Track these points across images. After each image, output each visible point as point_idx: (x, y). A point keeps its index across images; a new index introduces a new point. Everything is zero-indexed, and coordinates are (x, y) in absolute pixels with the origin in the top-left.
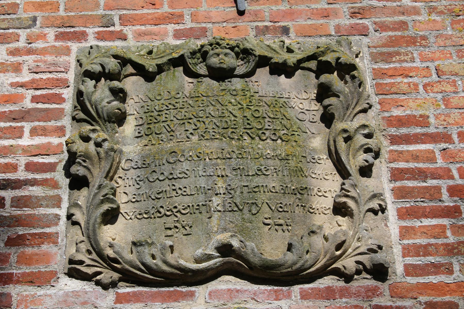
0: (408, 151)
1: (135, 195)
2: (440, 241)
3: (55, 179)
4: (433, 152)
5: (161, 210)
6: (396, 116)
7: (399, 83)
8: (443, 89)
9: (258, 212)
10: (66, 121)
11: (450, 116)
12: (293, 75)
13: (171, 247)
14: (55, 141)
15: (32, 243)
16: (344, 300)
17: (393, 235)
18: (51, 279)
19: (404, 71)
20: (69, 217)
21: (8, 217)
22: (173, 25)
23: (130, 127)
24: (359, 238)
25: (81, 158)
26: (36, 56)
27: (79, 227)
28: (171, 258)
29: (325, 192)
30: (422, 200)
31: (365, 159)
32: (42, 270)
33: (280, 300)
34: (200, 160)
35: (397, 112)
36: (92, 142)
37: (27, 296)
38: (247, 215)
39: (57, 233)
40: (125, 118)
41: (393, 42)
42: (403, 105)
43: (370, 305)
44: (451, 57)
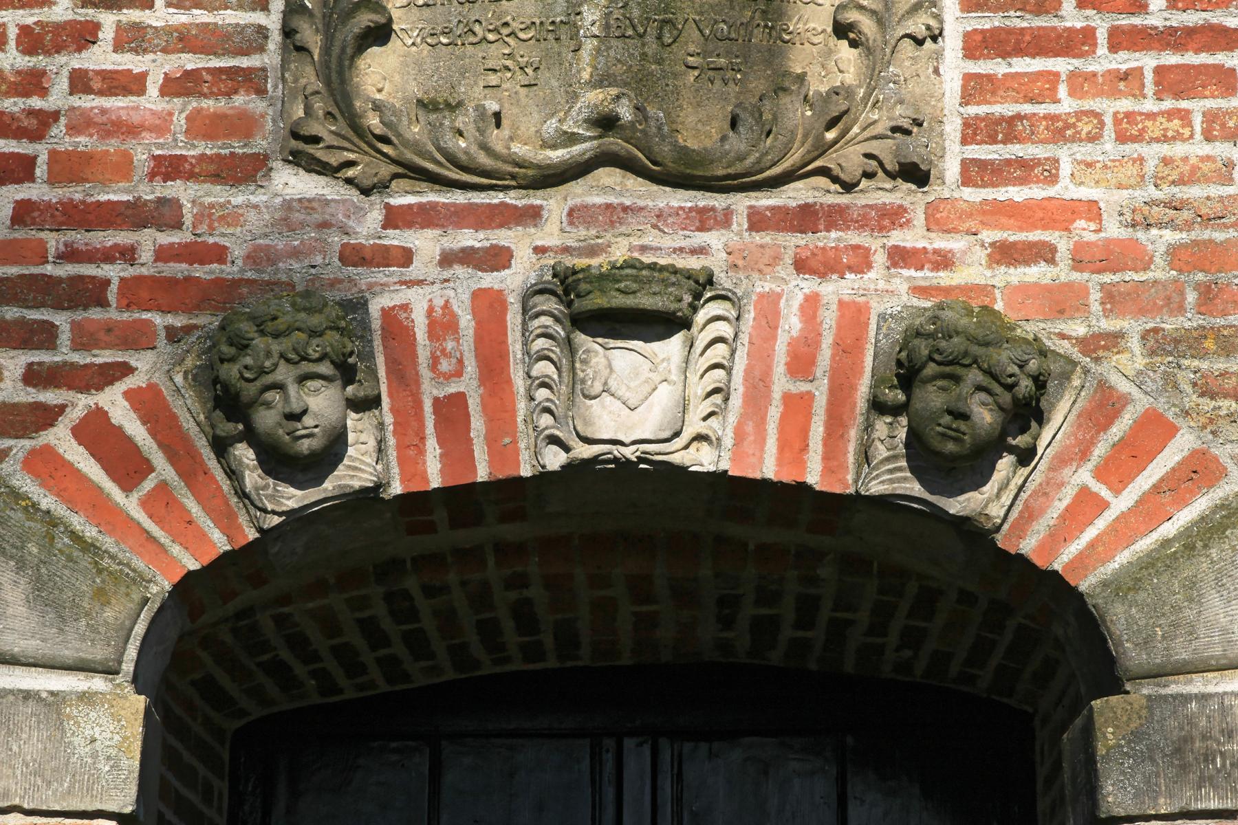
2: (1041, 109)
5: (477, 28)
9: (674, 41)
13: (497, 116)
15: (215, 90)
16: (834, 234)
17: (947, 95)
18: (257, 171)
20: (288, 32)
21: (163, 28)
27: (309, 59)
28: (497, 138)
30: (1018, 14)
32: (237, 150)
33: (709, 230)
37: (212, 206)
38: (652, 47)
39: (264, 69)
43: (884, 247)
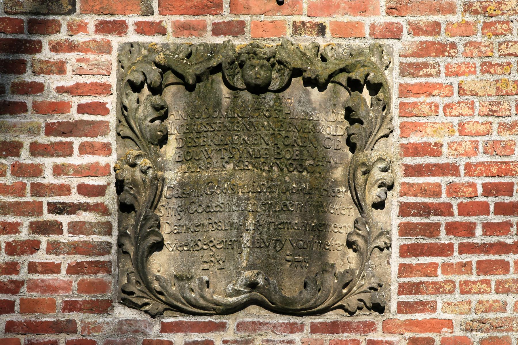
0: (418, 184)
1: (176, 226)
3: (105, 204)
4: (440, 186)
5: (199, 243)
6: (413, 144)
7: (421, 103)
8: (461, 112)
9: (281, 249)
10: (111, 138)
11: (461, 145)
12: (326, 88)
13: (208, 282)
14: (102, 160)
19: (428, 88)
20: (120, 245)
21: (67, 243)
22: (211, 16)
23: (171, 148)
24: (364, 276)
25: (128, 186)
26: (78, 53)
28: (207, 292)
29: (341, 228)
30: (422, 237)
31: (378, 194)
32: (100, 298)
33: (294, 333)
34: (234, 193)
35: (415, 139)
36: (137, 169)
37: (89, 323)
38: (272, 252)
39: (110, 262)
40: (167, 138)
41: (424, 50)
42: (421, 130)
43: (365, 340)
44: (475, 72)
